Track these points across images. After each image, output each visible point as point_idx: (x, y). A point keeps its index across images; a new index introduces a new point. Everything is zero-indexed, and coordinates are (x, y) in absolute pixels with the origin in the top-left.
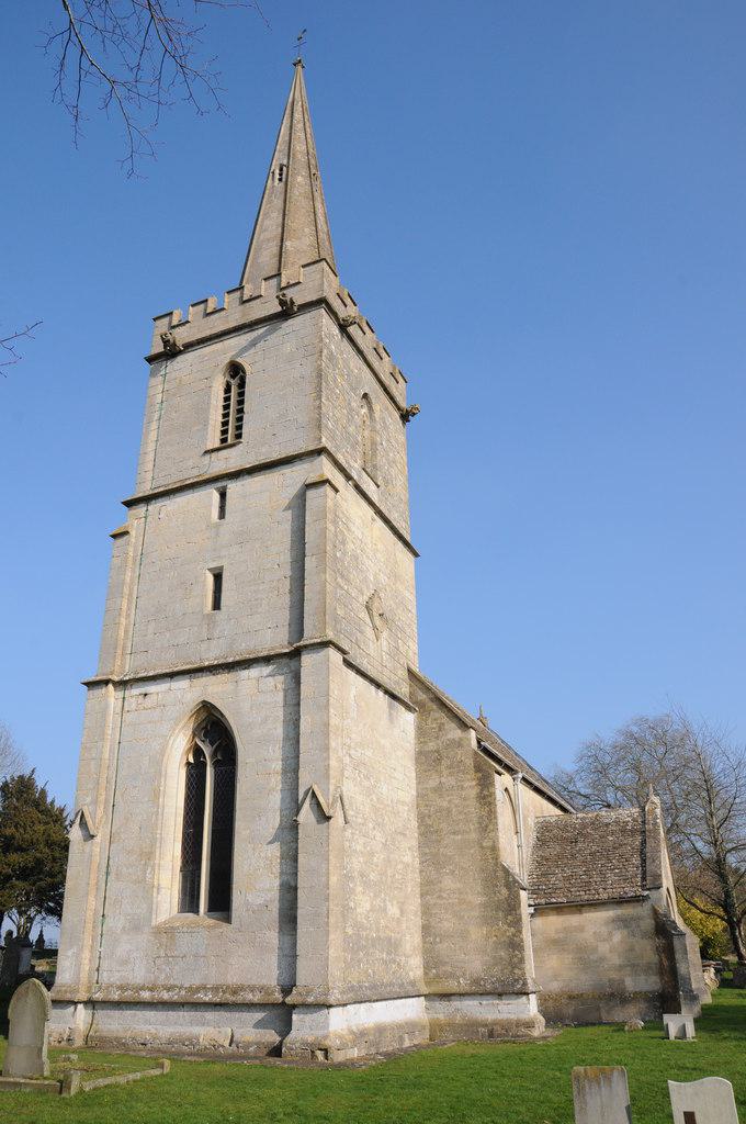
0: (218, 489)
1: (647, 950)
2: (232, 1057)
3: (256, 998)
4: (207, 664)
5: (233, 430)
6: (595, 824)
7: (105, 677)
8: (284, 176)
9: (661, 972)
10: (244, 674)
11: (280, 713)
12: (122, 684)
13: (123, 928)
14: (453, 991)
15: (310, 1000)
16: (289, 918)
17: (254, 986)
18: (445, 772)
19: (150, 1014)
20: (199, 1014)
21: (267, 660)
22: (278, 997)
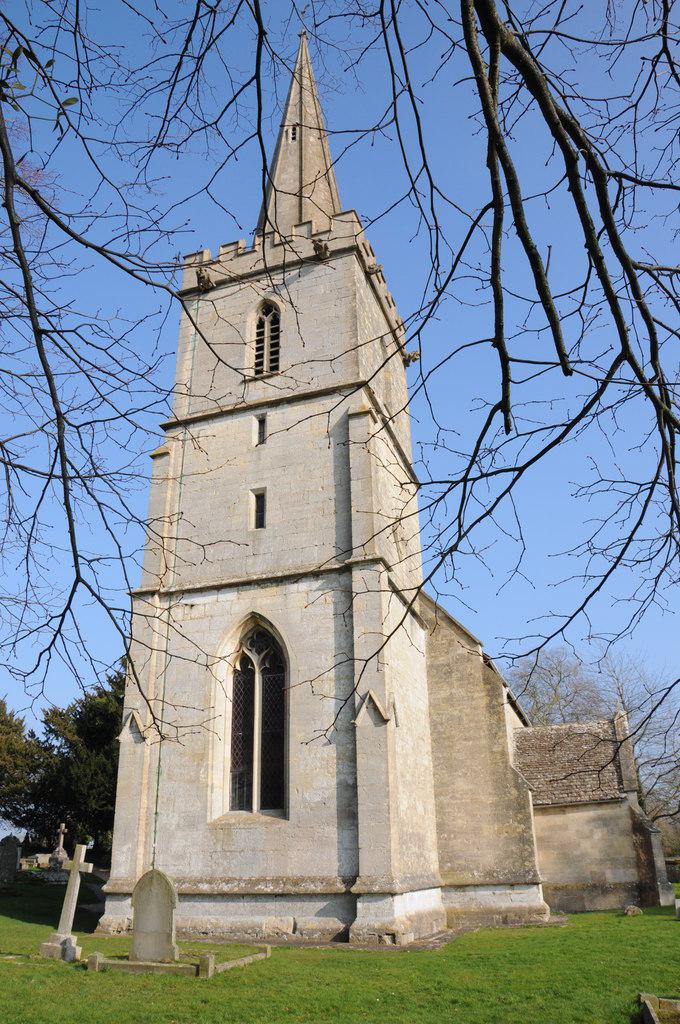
0: (256, 416)
1: (626, 846)
2: (298, 944)
3: (319, 888)
4: (255, 578)
5: (269, 362)
6: (569, 735)
7: (150, 589)
8: (297, 135)
9: (638, 865)
10: (293, 587)
11: (331, 624)
12: (169, 595)
13: (178, 825)
14: (469, 882)
15: (376, 889)
16: (349, 813)
17: (315, 878)
18: (456, 684)
19: (209, 905)
20: (259, 904)
21: (316, 574)
22: (341, 887)
